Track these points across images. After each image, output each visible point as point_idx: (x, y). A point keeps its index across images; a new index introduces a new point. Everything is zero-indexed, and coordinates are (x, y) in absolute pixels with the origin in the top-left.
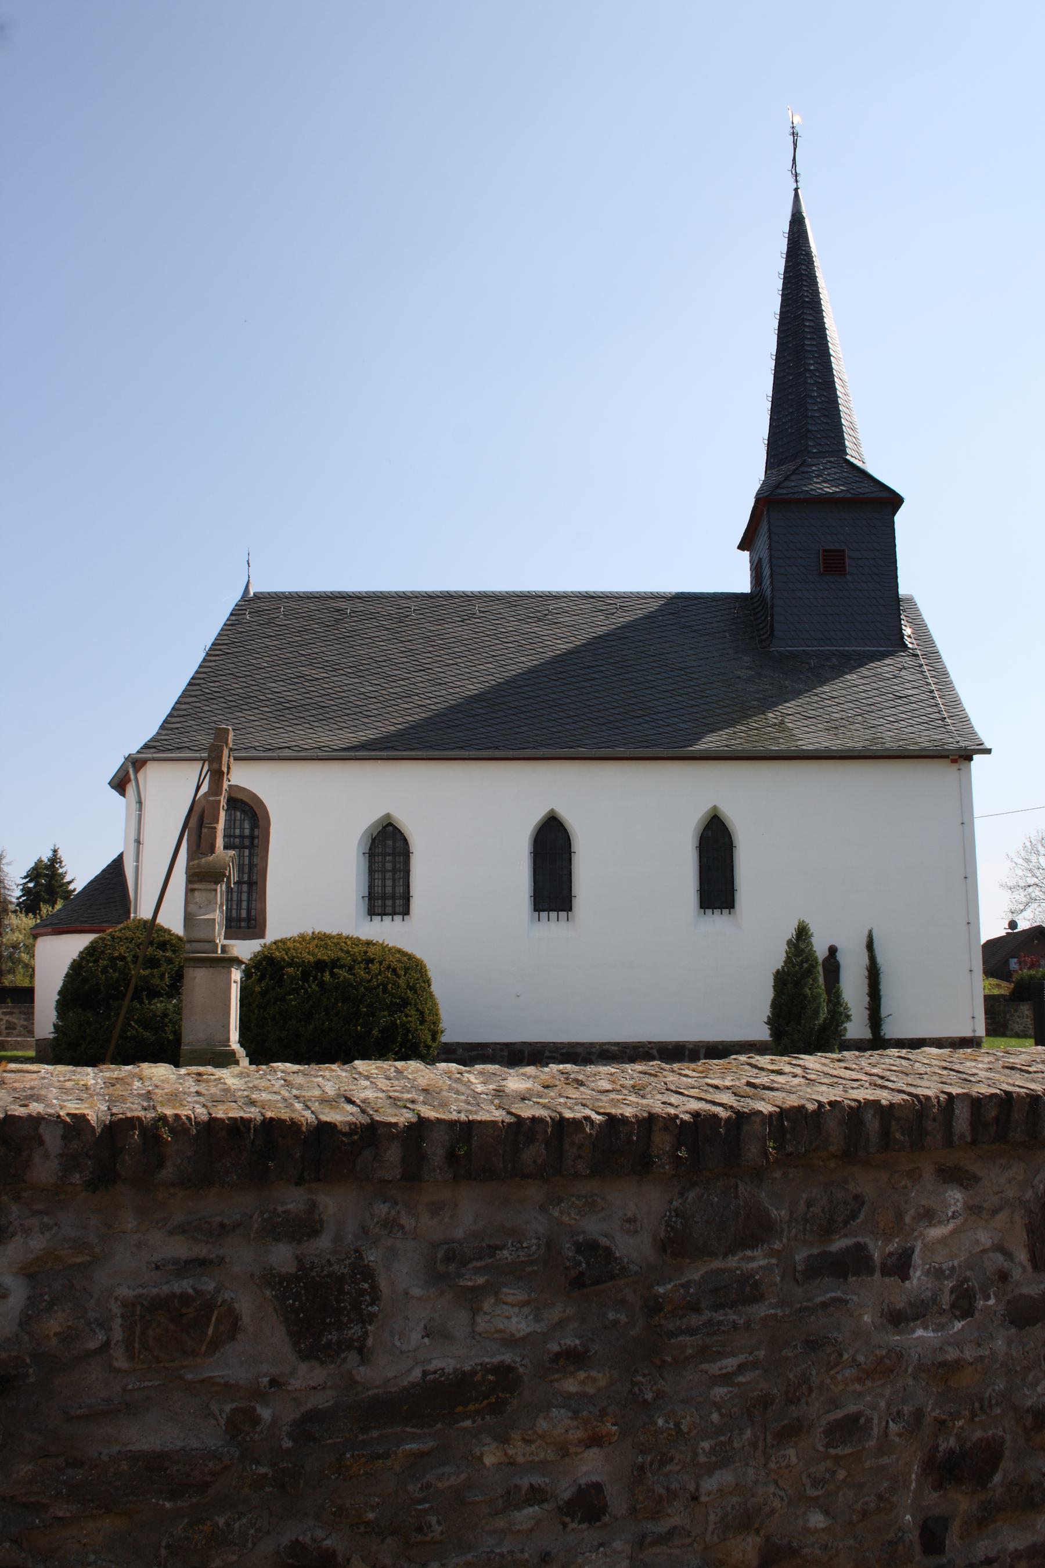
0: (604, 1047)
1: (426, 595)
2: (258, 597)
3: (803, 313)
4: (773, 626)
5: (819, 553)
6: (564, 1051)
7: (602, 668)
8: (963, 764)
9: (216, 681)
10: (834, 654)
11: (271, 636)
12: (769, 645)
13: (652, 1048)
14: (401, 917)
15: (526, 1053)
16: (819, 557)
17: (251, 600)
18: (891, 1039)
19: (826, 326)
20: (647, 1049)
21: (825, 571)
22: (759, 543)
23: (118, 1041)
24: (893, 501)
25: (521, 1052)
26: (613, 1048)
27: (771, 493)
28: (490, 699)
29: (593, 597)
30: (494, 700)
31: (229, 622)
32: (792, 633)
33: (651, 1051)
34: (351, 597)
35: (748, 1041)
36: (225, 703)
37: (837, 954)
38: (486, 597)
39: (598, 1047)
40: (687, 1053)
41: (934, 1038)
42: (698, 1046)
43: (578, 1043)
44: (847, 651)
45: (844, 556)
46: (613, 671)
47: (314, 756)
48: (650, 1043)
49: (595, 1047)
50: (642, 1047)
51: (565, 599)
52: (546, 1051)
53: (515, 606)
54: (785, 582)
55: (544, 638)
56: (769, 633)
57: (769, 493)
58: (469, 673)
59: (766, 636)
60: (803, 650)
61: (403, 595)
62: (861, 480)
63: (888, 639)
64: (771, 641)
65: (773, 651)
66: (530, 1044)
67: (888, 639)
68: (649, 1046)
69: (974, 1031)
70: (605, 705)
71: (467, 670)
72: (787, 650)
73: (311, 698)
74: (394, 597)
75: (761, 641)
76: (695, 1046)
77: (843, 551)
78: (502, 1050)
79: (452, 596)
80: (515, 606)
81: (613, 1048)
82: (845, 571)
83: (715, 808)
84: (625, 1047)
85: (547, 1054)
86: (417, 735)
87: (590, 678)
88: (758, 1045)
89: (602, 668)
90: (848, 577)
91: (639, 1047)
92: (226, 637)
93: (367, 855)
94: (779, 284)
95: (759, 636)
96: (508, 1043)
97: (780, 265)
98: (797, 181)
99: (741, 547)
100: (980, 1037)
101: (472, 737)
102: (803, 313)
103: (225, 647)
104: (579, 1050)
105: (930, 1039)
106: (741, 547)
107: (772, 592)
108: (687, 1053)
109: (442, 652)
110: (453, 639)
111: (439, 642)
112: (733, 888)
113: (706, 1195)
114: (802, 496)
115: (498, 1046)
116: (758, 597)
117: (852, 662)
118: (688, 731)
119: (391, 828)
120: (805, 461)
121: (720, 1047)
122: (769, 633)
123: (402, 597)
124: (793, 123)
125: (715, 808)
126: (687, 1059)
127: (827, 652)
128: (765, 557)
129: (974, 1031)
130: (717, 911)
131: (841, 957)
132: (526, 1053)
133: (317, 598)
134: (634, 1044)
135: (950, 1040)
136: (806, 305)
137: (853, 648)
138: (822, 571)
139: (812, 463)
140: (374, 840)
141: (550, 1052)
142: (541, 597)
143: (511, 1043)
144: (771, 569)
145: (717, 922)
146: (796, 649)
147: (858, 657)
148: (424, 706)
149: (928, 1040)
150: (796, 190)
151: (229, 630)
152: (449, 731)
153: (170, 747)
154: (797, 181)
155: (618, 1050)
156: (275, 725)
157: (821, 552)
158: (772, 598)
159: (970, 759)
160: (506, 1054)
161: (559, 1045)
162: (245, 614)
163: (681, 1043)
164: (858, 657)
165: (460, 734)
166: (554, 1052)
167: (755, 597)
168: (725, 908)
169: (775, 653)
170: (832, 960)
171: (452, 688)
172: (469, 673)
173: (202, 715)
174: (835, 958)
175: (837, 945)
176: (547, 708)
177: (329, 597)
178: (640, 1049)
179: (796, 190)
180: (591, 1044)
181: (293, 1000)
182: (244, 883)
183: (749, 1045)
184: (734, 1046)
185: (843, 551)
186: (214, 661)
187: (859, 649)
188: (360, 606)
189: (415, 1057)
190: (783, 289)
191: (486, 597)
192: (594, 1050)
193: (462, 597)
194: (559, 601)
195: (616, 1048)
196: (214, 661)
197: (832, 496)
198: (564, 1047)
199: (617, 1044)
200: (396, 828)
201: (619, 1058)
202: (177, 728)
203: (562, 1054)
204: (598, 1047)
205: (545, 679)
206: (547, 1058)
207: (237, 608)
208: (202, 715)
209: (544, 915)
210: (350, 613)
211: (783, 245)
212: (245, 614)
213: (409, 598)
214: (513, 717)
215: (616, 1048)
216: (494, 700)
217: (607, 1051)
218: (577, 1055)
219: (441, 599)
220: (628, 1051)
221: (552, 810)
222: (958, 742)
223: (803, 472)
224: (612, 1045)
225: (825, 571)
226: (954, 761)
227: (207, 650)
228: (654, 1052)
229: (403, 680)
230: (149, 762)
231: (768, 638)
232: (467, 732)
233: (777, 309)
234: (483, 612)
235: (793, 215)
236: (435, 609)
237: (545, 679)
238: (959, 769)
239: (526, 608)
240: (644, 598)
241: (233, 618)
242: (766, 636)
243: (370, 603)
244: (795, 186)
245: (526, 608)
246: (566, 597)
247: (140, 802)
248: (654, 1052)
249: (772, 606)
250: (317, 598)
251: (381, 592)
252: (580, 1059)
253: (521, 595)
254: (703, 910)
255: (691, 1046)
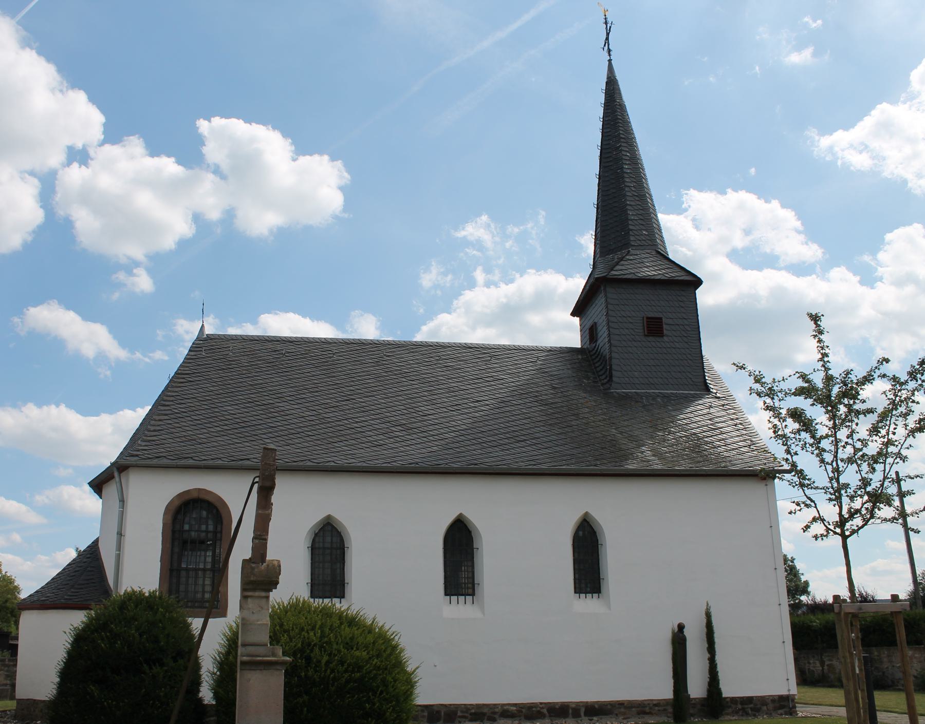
0: (505, 708)
2: (210, 338)
3: (620, 146)
4: (612, 373)
5: (643, 319)
6: (473, 711)
7: (487, 402)
8: (769, 482)
9: (183, 404)
10: (658, 396)
11: (224, 369)
12: (609, 388)
13: (543, 708)
14: (591, 595)
15: (443, 713)
16: (644, 326)
17: (205, 340)
18: (727, 698)
19: (224, 119)
20: (538, 709)
21: (648, 333)
22: (593, 312)
23: (13, 710)
25: (438, 712)
26: (512, 708)
29: (471, 348)
31: (188, 357)
32: (626, 379)
33: (542, 710)
34: (284, 341)
35: (618, 701)
36: (191, 421)
37: (685, 630)
38: (309, 342)
40: (570, 711)
41: (759, 697)
42: (579, 705)
43: (484, 705)
44: (667, 393)
45: (662, 322)
46: (496, 405)
47: (174, 465)
48: (541, 703)
50: (535, 707)
52: (459, 712)
53: (413, 352)
56: (608, 379)
58: (385, 403)
59: (606, 380)
60: (635, 392)
63: (695, 385)
65: (613, 392)
66: (445, 706)
67: (695, 385)
68: (541, 706)
69: (789, 690)
70: (495, 431)
71: (383, 401)
72: (623, 392)
73: (261, 420)
76: (577, 705)
77: (661, 319)
78: (423, 711)
79: (363, 343)
80: (413, 352)
81: (512, 708)
82: (663, 333)
83: (587, 514)
85: (459, 714)
88: (625, 705)
89: (487, 402)
90: (665, 338)
91: (532, 707)
92: (187, 369)
93: (310, 548)
97: (600, 112)
98: (610, 55)
102: (620, 146)
104: (485, 710)
105: (756, 697)
107: (610, 348)
108: (570, 711)
110: (323, 376)
111: (358, 378)
116: (594, 352)
119: (329, 528)
120: (629, 251)
123: (324, 342)
124: (605, 16)
125: (587, 514)
127: (653, 394)
128: (601, 321)
129: (789, 690)
132: (443, 713)
133: (257, 340)
134: (528, 705)
136: (622, 140)
138: (646, 334)
140: (316, 535)
141: (462, 712)
142: (431, 346)
143: (430, 705)
144: (609, 330)
145: (589, 604)
148: (353, 428)
149: (755, 698)
150: (610, 61)
154: (610, 55)
155: (516, 710)
156: (234, 440)
157: (645, 319)
158: (611, 352)
160: (426, 714)
161: (469, 706)
162: (202, 351)
163: (566, 704)
165: (385, 452)
168: (453, 595)
170: (681, 635)
171: (373, 415)
172: (385, 403)
173: (173, 430)
174: (682, 632)
176: (267, 428)
177: (267, 340)
178: (534, 709)
179: (610, 61)
180: (495, 705)
184: (607, 705)
185: (661, 319)
188: (292, 348)
189: (784, 697)
192: (497, 710)
193: (371, 344)
194: (445, 349)
195: (515, 708)
197: (652, 278)
198: (473, 708)
199: (515, 705)
200: (333, 527)
202: (153, 441)
203: (471, 714)
206: (460, 717)
208: (173, 430)
209: (454, 598)
211: (602, 98)
212: (202, 351)
213: (330, 343)
214: (425, 439)
215: (515, 708)
217: (507, 711)
218: (484, 714)
219: (355, 345)
220: (524, 710)
221: (461, 515)
222: (765, 464)
224: (511, 706)
225: (648, 333)
228: (545, 711)
229: (333, 407)
230: (131, 468)
232: (390, 450)
233: (599, 142)
235: (608, 78)
236: (351, 353)
238: (766, 485)
239: (422, 355)
241: (192, 353)
242: (606, 380)
244: (609, 58)
245: (422, 355)
246: (450, 347)
247: (122, 501)
248: (545, 711)
249: (611, 358)
250: (257, 340)
251: (307, 338)
252: (486, 718)
253: (416, 344)
255: (574, 706)
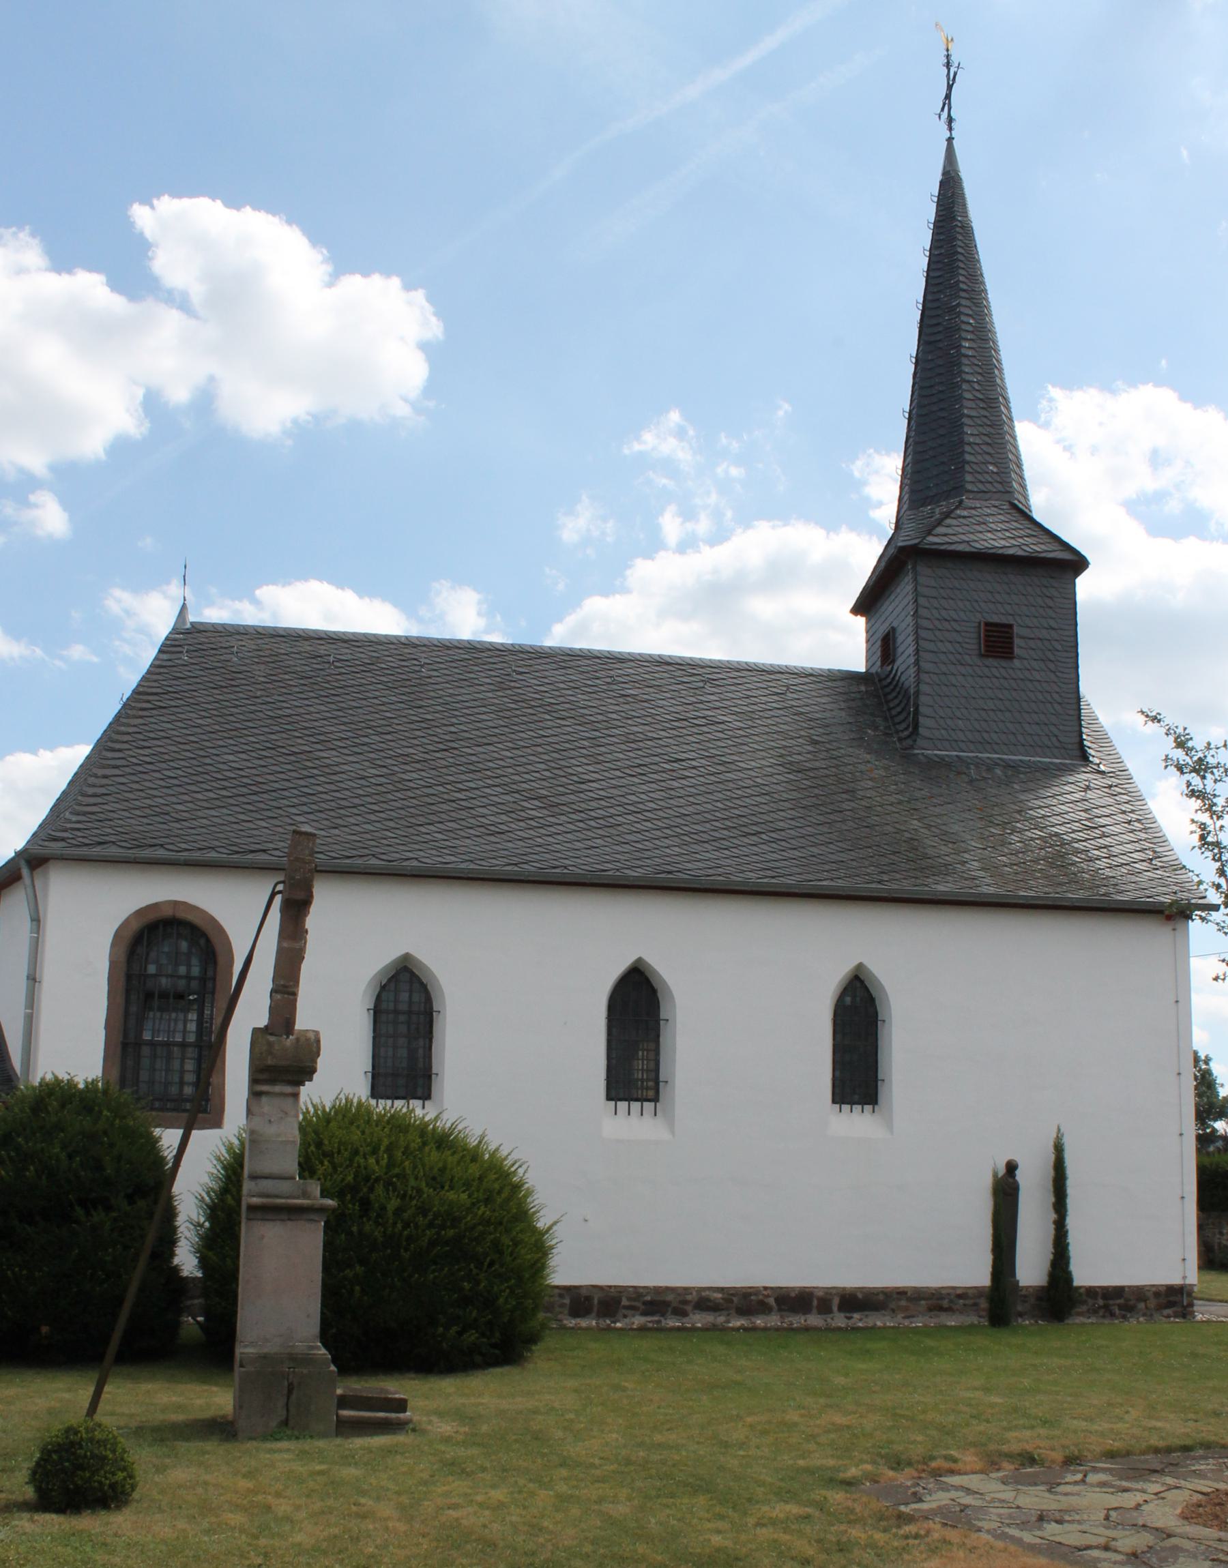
0: (703, 1294)
1: (439, 645)
6: (648, 1298)
7: (694, 763)
8: (1179, 925)
10: (997, 764)
11: (222, 687)
13: (768, 1296)
15: (596, 1301)
17: (187, 632)
22: (890, 609)
24: (1078, 564)
25: (588, 1299)
27: (922, 541)
28: (546, 797)
30: (551, 799)
32: (943, 732)
37: (1018, 1172)
39: (694, 1293)
40: (815, 1303)
42: (831, 1294)
48: (766, 1288)
49: (691, 1294)
51: (632, 664)
54: (935, 663)
55: (610, 715)
56: (911, 729)
57: (919, 540)
58: (512, 758)
59: (906, 733)
60: (957, 756)
61: (407, 642)
62: (1034, 533)
64: (915, 741)
67: (1064, 748)
69: (1184, 1278)
70: (706, 815)
72: (936, 755)
74: (393, 644)
75: (900, 740)
76: (827, 1293)
77: (1010, 626)
79: (475, 648)
84: (732, 1295)
85: (625, 1302)
86: (447, 843)
87: (297, 751)
88: (909, 1294)
89: (694, 763)
91: (750, 1294)
93: (372, 1012)
94: (924, 262)
95: (897, 732)
96: (571, 1286)
97: (925, 238)
98: (950, 129)
99: (859, 609)
100: (1190, 1285)
101: (528, 850)
103: (156, 698)
104: (670, 1297)
106: (859, 609)
107: (918, 674)
108: (815, 1303)
109: (470, 726)
112: (877, 1077)
113: (582, 1425)
114: (960, 548)
115: (557, 1291)
117: (1022, 776)
118: (822, 857)
120: (961, 502)
121: (860, 1296)
122: (911, 729)
123: (405, 644)
125: (860, 966)
126: (815, 1311)
127: (988, 761)
128: (904, 625)
129: (1184, 1278)
130: (857, 1108)
131: (1020, 1175)
132: (596, 1301)
135: (1154, 1289)
136: (963, 294)
137: (936, 752)
138: (983, 652)
139: (970, 505)
140: (383, 988)
141: (629, 1299)
142: (599, 658)
146: (947, 753)
147: (1028, 770)
149: (1126, 1289)
151: (159, 674)
152: (492, 839)
153: (87, 841)
154: (950, 129)
155: (723, 1299)
157: (982, 624)
159: (1189, 917)
160: (567, 1301)
161: (641, 1290)
163: (807, 1290)
164: (1028, 770)
165: (510, 845)
166: (635, 1300)
167: (885, 679)
169: (920, 757)
170: (1011, 1180)
175: (1009, 1157)
180: (686, 1289)
181: (406, 1255)
182: (190, 1045)
183: (898, 1293)
184: (878, 1294)
185: (1010, 626)
186: (141, 717)
187: (1028, 758)
190: (928, 271)
191: (522, 652)
192: (689, 1298)
193: (490, 650)
195: (720, 1295)
196: (141, 717)
198: (648, 1293)
200: (412, 974)
201: (723, 1309)
203: (645, 1303)
204: (694, 1293)
205: (618, 773)
207: (168, 642)
209: (622, 1105)
210: (333, 661)
212: (182, 652)
213: (415, 646)
215: (720, 1295)
216: (551, 799)
217: (708, 1299)
218: (666, 1304)
219: (461, 651)
220: (735, 1299)
222: (1175, 893)
223: (960, 517)
225: (986, 651)
226: (1169, 918)
227: (124, 700)
228: (771, 1301)
230: (51, 861)
231: (909, 737)
234: (521, 673)
237: (618, 773)
238: (1174, 930)
240: (738, 670)
241: (165, 657)
242: (906, 733)
243: (361, 650)
244: (949, 135)
246: (632, 661)
248: (771, 1301)
249: (917, 693)
253: (570, 653)
254: (838, 1106)
255: (821, 1294)
